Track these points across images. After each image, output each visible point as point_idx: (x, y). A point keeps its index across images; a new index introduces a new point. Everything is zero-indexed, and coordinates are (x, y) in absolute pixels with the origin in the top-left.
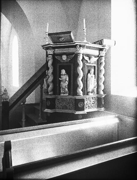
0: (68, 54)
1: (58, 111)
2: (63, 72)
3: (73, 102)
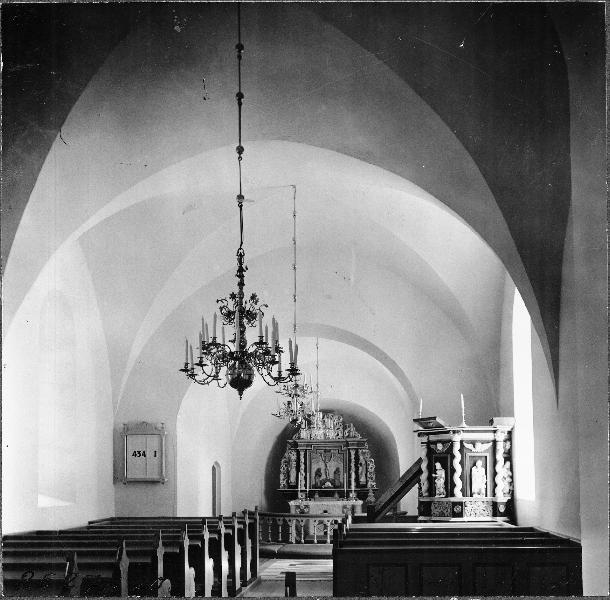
0: (443, 442)
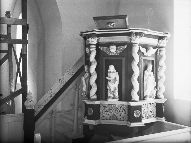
0: (118, 45)
1: (103, 122)
2: (112, 68)
3: (126, 110)
